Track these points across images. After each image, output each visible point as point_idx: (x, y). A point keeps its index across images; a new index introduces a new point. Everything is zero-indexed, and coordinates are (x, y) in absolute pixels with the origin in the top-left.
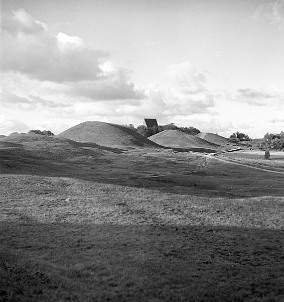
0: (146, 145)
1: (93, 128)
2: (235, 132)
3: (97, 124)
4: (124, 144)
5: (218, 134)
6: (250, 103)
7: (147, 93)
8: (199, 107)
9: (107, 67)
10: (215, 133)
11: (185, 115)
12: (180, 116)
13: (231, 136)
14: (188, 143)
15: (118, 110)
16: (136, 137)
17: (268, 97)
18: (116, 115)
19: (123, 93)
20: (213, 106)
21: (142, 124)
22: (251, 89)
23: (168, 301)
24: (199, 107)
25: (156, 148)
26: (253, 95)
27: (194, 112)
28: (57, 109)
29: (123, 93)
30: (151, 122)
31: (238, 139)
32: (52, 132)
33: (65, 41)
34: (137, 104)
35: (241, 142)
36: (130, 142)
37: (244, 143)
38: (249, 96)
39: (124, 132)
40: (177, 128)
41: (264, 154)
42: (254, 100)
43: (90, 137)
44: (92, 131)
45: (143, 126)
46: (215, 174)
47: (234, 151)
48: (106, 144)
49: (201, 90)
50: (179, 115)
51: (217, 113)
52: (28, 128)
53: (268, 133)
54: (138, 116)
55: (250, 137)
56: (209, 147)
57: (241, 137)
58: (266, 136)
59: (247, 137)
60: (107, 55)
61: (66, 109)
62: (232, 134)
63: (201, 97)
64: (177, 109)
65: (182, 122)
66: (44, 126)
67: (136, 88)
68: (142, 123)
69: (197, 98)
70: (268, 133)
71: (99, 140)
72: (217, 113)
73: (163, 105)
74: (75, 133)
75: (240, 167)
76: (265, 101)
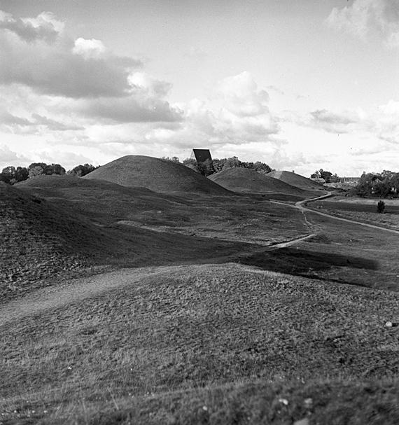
3: (143, 160)
4: (185, 189)
6: (329, 130)
7: (188, 114)
8: (259, 134)
9: (137, 79)
10: (291, 171)
11: (238, 144)
12: (230, 146)
13: (313, 176)
15: (148, 137)
17: (347, 122)
18: (145, 142)
19: (163, 116)
20: (275, 132)
21: (189, 158)
22: (327, 111)
23: (144, 424)
24: (259, 134)
25: (226, 195)
26: (328, 120)
27: (250, 140)
28: (67, 133)
29: (163, 116)
31: (323, 180)
32: (63, 166)
33: (85, 46)
34: (172, 128)
35: (328, 185)
37: (332, 185)
38: (323, 119)
41: (377, 203)
42: (334, 126)
43: (136, 178)
47: (325, 198)
49: (263, 111)
50: (230, 143)
51: (284, 142)
52: (30, 161)
53: (364, 172)
54: (183, 146)
55: (340, 176)
58: (364, 175)
60: (137, 64)
61: (79, 132)
62: (313, 173)
63: (263, 121)
64: (229, 136)
66: (97, 163)
67: (173, 105)
69: (254, 121)
70: (364, 172)
71: (148, 183)
72: (284, 142)
73: (211, 131)
75: (365, 228)
76: (341, 127)
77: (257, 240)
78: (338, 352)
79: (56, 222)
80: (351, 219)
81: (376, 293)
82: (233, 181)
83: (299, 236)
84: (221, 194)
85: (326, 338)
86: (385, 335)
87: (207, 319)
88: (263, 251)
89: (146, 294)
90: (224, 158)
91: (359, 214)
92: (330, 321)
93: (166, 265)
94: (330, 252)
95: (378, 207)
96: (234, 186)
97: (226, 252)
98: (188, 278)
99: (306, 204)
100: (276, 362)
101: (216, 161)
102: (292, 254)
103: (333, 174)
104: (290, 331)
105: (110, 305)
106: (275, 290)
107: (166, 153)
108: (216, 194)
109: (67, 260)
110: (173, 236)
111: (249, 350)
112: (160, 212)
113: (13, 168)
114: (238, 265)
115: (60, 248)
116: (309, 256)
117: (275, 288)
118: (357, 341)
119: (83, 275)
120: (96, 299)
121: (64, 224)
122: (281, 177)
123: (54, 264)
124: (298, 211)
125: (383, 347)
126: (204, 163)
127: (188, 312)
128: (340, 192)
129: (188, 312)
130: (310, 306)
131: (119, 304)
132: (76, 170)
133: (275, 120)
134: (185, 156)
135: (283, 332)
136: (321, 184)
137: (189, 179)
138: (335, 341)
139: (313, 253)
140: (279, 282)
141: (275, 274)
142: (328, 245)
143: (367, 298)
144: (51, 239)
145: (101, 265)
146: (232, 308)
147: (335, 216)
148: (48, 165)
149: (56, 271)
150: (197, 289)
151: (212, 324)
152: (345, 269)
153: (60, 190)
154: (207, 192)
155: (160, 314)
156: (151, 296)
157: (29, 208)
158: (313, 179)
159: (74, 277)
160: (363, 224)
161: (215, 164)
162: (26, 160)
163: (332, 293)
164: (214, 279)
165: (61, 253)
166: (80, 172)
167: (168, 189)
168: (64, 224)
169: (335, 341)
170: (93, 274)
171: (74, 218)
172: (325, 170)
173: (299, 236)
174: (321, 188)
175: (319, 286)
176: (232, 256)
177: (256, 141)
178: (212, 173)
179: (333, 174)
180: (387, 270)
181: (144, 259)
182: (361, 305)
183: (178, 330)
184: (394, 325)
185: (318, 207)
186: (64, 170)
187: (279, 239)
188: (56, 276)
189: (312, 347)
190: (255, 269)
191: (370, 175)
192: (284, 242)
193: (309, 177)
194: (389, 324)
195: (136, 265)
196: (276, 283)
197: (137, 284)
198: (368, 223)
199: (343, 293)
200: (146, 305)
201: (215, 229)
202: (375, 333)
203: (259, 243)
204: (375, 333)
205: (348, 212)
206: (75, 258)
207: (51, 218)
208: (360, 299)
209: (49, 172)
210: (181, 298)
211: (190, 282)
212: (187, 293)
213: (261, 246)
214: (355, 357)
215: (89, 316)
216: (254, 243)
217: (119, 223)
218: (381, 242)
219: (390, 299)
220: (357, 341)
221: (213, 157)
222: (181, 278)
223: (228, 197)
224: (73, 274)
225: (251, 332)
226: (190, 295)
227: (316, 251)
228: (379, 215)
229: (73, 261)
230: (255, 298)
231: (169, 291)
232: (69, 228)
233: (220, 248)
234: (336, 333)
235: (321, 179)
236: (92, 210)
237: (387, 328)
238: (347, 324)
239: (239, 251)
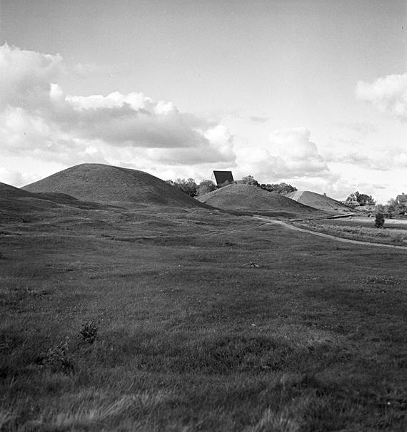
2: (354, 192)
75: (402, 252)
172: (361, 193)
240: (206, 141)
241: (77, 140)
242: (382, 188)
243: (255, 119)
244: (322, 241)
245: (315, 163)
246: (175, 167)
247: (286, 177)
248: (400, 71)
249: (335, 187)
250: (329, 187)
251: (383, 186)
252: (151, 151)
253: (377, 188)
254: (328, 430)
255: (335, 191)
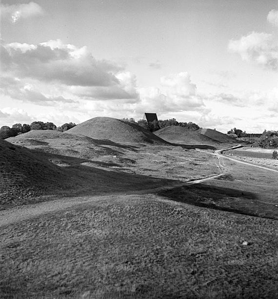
0: (156, 142)
1: (104, 124)
2: (233, 128)
3: (108, 120)
4: (136, 141)
5: (216, 130)
10: (213, 129)
13: (229, 133)
14: (192, 139)
16: (145, 134)
21: (142, 119)
25: (165, 145)
30: (151, 117)
32: (54, 124)
36: (141, 139)
37: (242, 139)
39: (134, 128)
40: (177, 124)
41: (272, 153)
43: (102, 133)
44: (104, 127)
45: (144, 121)
46: (241, 178)
48: (118, 140)
53: (265, 130)
55: (249, 131)
56: (212, 144)
57: (238, 132)
58: (265, 132)
59: (245, 133)
62: (230, 130)
65: (182, 117)
68: (143, 118)
70: (265, 130)
71: (111, 136)
74: (87, 128)
75: (261, 170)
77: (180, 177)
78: (195, 265)
79: (24, 163)
80: (252, 163)
81: (246, 219)
82: (171, 136)
83: (212, 175)
84: (161, 144)
85: (190, 254)
86: (238, 252)
87: (107, 237)
88: (183, 184)
89: (70, 216)
90: (166, 119)
91: (259, 160)
92: (200, 240)
93: (99, 195)
94: (231, 187)
95: (273, 155)
96: (172, 139)
97: (154, 185)
98: (107, 205)
99: (222, 153)
100: (143, 274)
101: (161, 121)
102: (199, 188)
103: (243, 131)
104: (166, 248)
105: (40, 225)
106: (169, 216)
107: (129, 116)
108: (158, 144)
109: (23, 190)
110: (118, 174)
111: (127, 262)
112: (115, 156)
113: (20, 125)
114: (154, 196)
115: (20, 182)
116: (215, 189)
117: (170, 213)
118: (215, 256)
119: (31, 202)
120: (32, 221)
121: (29, 165)
122: (206, 133)
123: (13, 194)
124: (216, 157)
125: (233, 262)
126: (152, 123)
127: (95, 231)
128: (247, 144)
129: (95, 231)
130: (191, 228)
131: (47, 225)
132: (63, 127)
133: (200, 97)
134: (139, 118)
135: (160, 249)
136: (234, 138)
137: (140, 133)
138: (197, 256)
139: (218, 187)
140: (175, 210)
141: (176, 203)
142: (232, 182)
143: (238, 222)
144: (15, 175)
145: (49, 195)
146: (130, 229)
147: (241, 160)
148: (44, 123)
149: (12, 199)
150: (110, 214)
151: (109, 241)
152: (237, 199)
153: (46, 141)
154: (152, 143)
155: (73, 232)
156: (74, 219)
157: (5, 153)
158: (229, 135)
159: (25, 204)
160: (260, 167)
161: (160, 123)
162: (29, 119)
163: (212, 218)
164: (126, 207)
165: (20, 186)
166: (66, 128)
167: (124, 141)
168: (29, 165)
169: (197, 256)
170: (40, 201)
171: (38, 160)
172: (237, 129)
173: (212, 175)
174: (234, 141)
175: (205, 213)
176: (158, 189)
177: (186, 110)
178: (158, 129)
179: (243, 131)
180: (270, 201)
181: (85, 190)
182: (231, 227)
183: (81, 245)
184: (249, 244)
185: (230, 154)
186: (56, 126)
187: (197, 177)
188: (11, 202)
189: (176, 261)
190: (165, 199)
191: (269, 132)
192: (200, 179)
193: (227, 133)
194: (245, 243)
195: (77, 195)
196: (172, 210)
197: (68, 209)
198: (264, 166)
199: (220, 219)
200: (66, 225)
201: (152, 169)
202: (231, 250)
203: (181, 179)
204: (231, 250)
205: (251, 159)
206: (29, 190)
207: (20, 161)
208: (232, 223)
209: (45, 128)
210: (96, 221)
211: (108, 209)
212: (101, 217)
213: (182, 182)
214: (206, 269)
215: (20, 234)
216: (177, 179)
217: (82, 164)
218: (271, 180)
219: (255, 224)
220: (215, 256)
221: (159, 119)
222: (102, 206)
223: (167, 147)
224: (24, 201)
225: (135, 248)
226: (103, 218)
227: (221, 186)
228: (273, 161)
229: (27, 192)
230: (151, 221)
231: (88, 215)
232: (32, 167)
233: (150, 183)
234: (201, 250)
235: (234, 135)
236: (67, 155)
237: (242, 247)
238: (212, 242)
239: (164, 185)
240: (117, 81)
241: (17, 79)
242: (241, 120)
243: (152, 65)
244: (241, 166)
245: (194, 100)
246: (95, 101)
247: (208, 126)
248: (262, 26)
249: (207, 118)
250: (203, 118)
251: (240, 118)
252: (73, 88)
253: (236, 119)
254: (178, 298)
255: (207, 121)
